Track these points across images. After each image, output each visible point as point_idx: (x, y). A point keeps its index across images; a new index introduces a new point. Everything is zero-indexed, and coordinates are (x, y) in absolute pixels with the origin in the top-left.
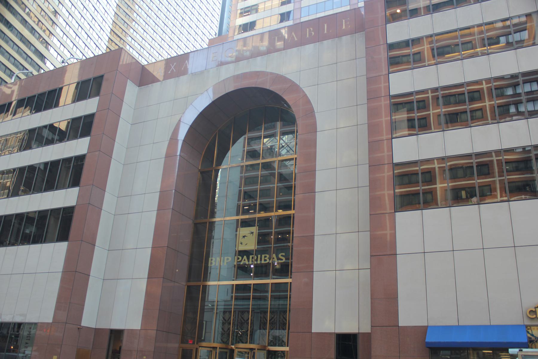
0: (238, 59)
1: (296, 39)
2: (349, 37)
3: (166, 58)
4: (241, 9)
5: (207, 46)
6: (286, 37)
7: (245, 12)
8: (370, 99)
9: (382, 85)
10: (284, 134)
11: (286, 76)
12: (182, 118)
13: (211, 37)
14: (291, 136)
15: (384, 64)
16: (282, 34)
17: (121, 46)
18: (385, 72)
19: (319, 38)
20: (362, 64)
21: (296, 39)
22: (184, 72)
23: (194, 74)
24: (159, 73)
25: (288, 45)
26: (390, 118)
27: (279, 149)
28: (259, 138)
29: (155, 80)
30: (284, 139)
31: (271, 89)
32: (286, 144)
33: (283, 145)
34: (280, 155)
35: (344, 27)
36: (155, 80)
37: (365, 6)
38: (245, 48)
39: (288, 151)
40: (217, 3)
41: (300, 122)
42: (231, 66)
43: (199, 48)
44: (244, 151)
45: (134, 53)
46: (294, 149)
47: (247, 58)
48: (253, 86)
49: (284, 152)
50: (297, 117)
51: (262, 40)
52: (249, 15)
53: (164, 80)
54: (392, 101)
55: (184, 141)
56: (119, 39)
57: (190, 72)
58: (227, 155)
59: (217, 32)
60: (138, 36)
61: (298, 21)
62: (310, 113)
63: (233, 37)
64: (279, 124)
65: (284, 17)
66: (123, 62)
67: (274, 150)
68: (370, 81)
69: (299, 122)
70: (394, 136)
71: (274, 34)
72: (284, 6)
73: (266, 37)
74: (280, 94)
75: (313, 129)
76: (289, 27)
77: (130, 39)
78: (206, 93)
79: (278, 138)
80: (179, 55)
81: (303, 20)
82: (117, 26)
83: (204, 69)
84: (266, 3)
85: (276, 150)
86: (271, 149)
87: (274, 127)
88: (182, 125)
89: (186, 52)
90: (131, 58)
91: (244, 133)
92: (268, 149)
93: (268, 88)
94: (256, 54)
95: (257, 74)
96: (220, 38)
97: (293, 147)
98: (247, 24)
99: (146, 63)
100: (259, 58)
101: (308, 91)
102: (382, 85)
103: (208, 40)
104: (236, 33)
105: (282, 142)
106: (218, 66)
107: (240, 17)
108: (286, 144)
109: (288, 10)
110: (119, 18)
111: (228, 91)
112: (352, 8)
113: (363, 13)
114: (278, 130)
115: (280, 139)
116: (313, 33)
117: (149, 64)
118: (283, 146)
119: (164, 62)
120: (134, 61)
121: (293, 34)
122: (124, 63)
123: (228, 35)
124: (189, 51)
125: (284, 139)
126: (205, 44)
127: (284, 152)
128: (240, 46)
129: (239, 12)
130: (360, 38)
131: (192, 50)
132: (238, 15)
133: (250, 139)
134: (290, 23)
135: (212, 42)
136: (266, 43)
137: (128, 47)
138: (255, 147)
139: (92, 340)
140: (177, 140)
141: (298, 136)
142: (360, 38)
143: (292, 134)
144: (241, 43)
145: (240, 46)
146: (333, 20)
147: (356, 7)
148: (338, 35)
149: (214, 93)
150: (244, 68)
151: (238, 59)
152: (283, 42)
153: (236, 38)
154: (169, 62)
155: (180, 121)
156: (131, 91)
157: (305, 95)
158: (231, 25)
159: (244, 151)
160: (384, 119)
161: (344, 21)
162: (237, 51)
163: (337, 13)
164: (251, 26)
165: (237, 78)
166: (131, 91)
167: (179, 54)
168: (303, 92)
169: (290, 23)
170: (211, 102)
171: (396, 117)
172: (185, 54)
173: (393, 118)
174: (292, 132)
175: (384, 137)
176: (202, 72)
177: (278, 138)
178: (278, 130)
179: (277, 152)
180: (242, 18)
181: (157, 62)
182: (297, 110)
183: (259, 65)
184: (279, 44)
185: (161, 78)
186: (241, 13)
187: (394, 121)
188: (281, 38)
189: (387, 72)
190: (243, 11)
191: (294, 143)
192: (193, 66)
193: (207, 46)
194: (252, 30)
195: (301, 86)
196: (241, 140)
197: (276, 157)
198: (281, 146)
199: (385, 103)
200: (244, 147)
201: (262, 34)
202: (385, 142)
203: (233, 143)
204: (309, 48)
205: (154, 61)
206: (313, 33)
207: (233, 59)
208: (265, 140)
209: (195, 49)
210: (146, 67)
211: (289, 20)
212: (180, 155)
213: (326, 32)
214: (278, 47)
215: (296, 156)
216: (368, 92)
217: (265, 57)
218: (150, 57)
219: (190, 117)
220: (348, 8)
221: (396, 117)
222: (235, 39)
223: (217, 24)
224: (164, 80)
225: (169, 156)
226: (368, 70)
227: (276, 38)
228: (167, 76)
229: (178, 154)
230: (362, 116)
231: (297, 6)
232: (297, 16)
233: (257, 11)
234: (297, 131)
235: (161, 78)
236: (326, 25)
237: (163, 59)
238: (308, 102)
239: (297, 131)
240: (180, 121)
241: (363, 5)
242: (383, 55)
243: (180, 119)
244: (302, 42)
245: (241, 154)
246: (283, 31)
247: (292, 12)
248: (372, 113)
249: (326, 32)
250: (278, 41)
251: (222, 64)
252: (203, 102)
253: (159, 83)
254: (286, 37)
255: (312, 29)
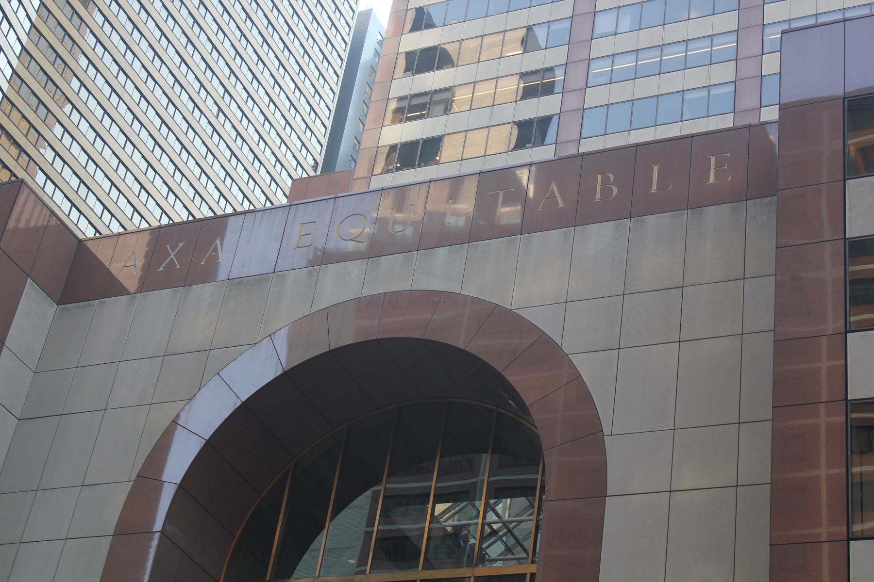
0: (378, 248)
1: (561, 205)
2: (725, 209)
3: (155, 224)
4: (401, 99)
5: (284, 201)
6: (531, 194)
7: (412, 109)
8: (781, 407)
9: (824, 365)
10: (499, 492)
11: (519, 312)
12: (183, 416)
13: (299, 173)
14: (522, 501)
15: (832, 302)
16: (517, 181)
17: (21, 174)
18: (834, 324)
19: (631, 205)
20: (762, 295)
21: (561, 205)
22: (208, 274)
23: (238, 283)
24: (127, 267)
25: (531, 223)
26: (844, 470)
27: (483, 539)
28: (421, 498)
29: (111, 287)
30: (499, 508)
31: (472, 348)
32: (505, 524)
33: (495, 526)
34: (482, 559)
35: (712, 179)
36: (111, 287)
37: (781, 122)
38: (399, 216)
39: (509, 550)
40: (330, 74)
41: (555, 460)
42: (355, 268)
43: (260, 201)
44: (369, 534)
45: (59, 197)
46: (529, 544)
47: (406, 248)
48: (418, 335)
49: (495, 550)
50: (545, 444)
51: (454, 196)
52: (422, 117)
53: (140, 290)
54: (854, 415)
55: (183, 487)
56: (15, 151)
57: (222, 274)
58: (312, 546)
59: (320, 160)
60: (76, 149)
61: (571, 150)
62: (589, 434)
63: (368, 179)
64: (486, 461)
65: (530, 132)
66: (18, 220)
67: (466, 540)
68: (785, 349)
69: (552, 459)
70: (857, 528)
71: (495, 183)
72: (533, 101)
73: (470, 189)
74: (498, 365)
75: (594, 486)
76: (543, 166)
77: (49, 154)
78: (267, 342)
79: (481, 505)
80: (196, 220)
81: (588, 146)
82: (15, 112)
83: (268, 268)
84: (479, 87)
85: (472, 541)
86: (457, 535)
87: (472, 469)
88: (180, 435)
89: (220, 213)
90: (49, 213)
91: (378, 481)
92: (447, 536)
93: (461, 345)
94: (433, 237)
95: (432, 298)
96: (324, 185)
97: (527, 537)
98: (415, 143)
99: (90, 233)
100: (442, 252)
101: (584, 365)
102: (824, 365)
103: (289, 182)
104: (378, 170)
105: (491, 517)
106: (311, 264)
107: (394, 122)
108: (505, 524)
109: (542, 113)
110: (24, 90)
111: (335, 344)
112: (741, 123)
113: (774, 137)
114: (484, 479)
115: (488, 507)
116: (615, 190)
117: (100, 236)
118: (494, 532)
119: (147, 237)
120: (54, 222)
121: (554, 186)
122: (22, 225)
123: (353, 171)
124: (229, 210)
125: (499, 508)
126: (280, 193)
127: (495, 550)
128: (385, 208)
129: (393, 105)
130: (761, 216)
131: (239, 209)
132: (389, 115)
133: (394, 502)
134: (544, 153)
135: (301, 190)
136: (466, 205)
137: (40, 178)
138: (406, 526)
139: (769, 199)
140: (159, 484)
141: (545, 506)
142: (761, 216)
143: (525, 495)
144: (387, 202)
145: (385, 208)
146: (679, 153)
147: (754, 121)
148: (692, 201)
149: (292, 345)
150: (393, 276)
151: (378, 248)
152: (519, 207)
153: (378, 182)
154: (162, 237)
155: (175, 422)
156: (34, 309)
157: (577, 378)
158: (366, 142)
159: (369, 534)
160: (825, 472)
161: (713, 159)
162: (376, 220)
163: (692, 136)
164: (422, 152)
165: (366, 305)
166: (34, 309)
167: (199, 216)
168: (572, 365)
169: (544, 153)
170: (280, 372)
171: (865, 468)
172: (216, 217)
173: (856, 470)
174: (525, 490)
175: (824, 531)
176: (261, 279)
177: (481, 505)
178: (484, 479)
179: (473, 547)
180: (399, 126)
181: (126, 233)
182: (548, 421)
183: (437, 272)
184: (508, 213)
185: (131, 285)
186: (398, 111)
187: (857, 480)
188: (515, 193)
189: (841, 324)
190: (405, 104)
191: (532, 525)
192: (235, 257)
193: (284, 201)
194: (427, 164)
195: (566, 349)
196: (363, 501)
197: (470, 564)
198: (488, 530)
199: (827, 421)
200: (370, 523)
201: (456, 182)
202: (826, 549)
203: (335, 513)
204: (600, 236)
205: (116, 228)
206: (615, 190)
207: (363, 246)
208: (440, 508)
209: (246, 206)
210: (89, 245)
211: (542, 143)
212: (162, 532)
213: (654, 189)
214: (504, 221)
215: (532, 568)
216: (780, 383)
217: (462, 251)
218: (107, 216)
219: (208, 412)
220: (727, 122)
221: (865, 468)
222: (372, 187)
223: (322, 133)
224: (140, 290)
225: (130, 528)
226: (781, 313)
227: (501, 194)
228: (152, 279)
229: (158, 526)
230: (755, 458)
231: (573, 102)
232: (570, 132)
233: (447, 110)
234: (543, 488)
235: (131, 285)
236: (656, 169)
237: (144, 225)
238: (586, 398)
239: (543, 488)
240: (175, 422)
241: (776, 116)
242: (831, 272)
243: (178, 416)
244: (579, 216)
245: (359, 544)
246: (524, 175)
247: (555, 120)
248: (788, 450)
249: (654, 189)
250: (506, 202)
251: (325, 258)
252: (254, 371)
253: (124, 299)
254: (531, 194)
255: (612, 178)
